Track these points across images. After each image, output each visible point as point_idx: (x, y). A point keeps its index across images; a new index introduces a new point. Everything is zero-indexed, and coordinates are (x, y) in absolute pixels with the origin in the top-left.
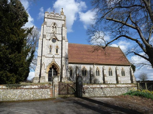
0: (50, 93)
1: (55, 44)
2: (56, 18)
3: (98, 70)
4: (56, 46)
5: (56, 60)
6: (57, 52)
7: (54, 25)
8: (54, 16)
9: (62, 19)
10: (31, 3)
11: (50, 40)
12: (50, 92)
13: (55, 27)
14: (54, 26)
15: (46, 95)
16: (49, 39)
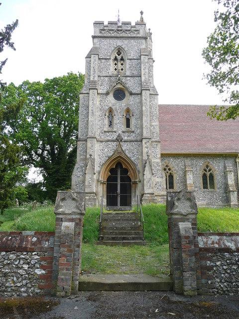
0: (39, 272)
1: (123, 105)
2: (124, 35)
3: (208, 174)
4: (125, 108)
5: (125, 146)
6: (128, 125)
7: (119, 55)
8: (118, 30)
9: (138, 35)
10: (152, 85)
11: (107, 94)
12: (42, 267)
13: (122, 59)
14: (119, 57)
15: (24, 282)
16: (105, 91)
